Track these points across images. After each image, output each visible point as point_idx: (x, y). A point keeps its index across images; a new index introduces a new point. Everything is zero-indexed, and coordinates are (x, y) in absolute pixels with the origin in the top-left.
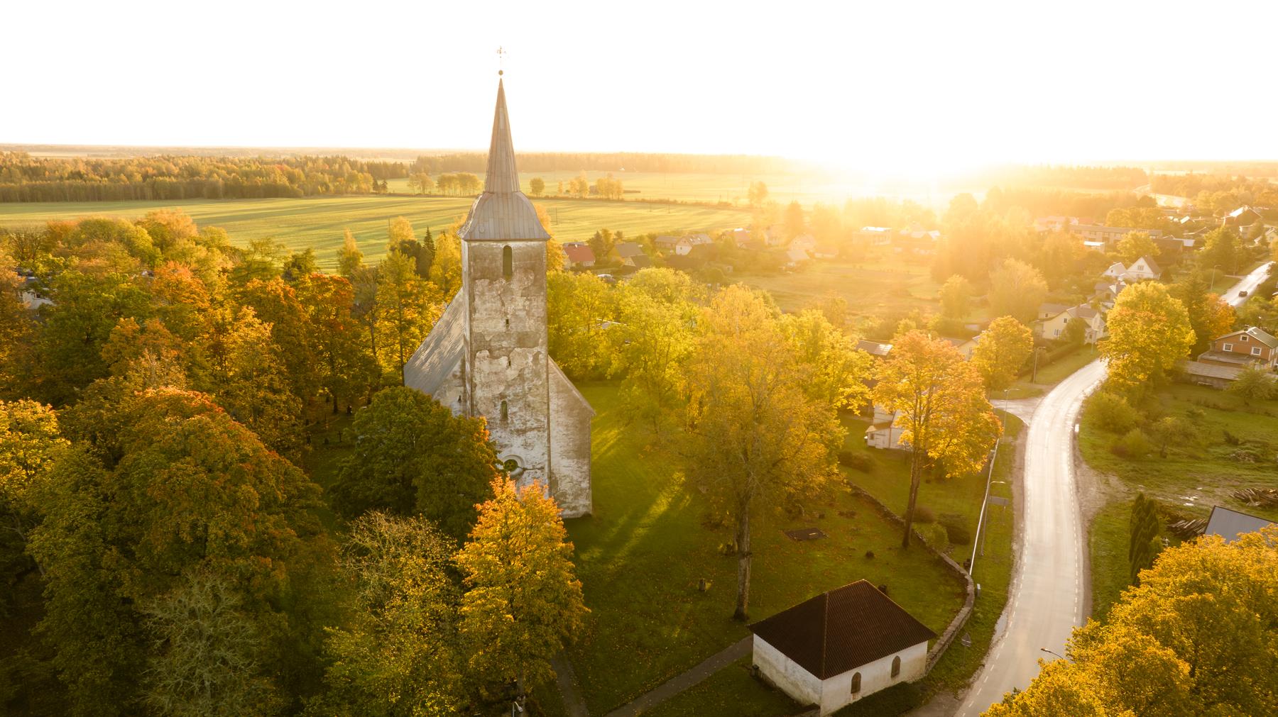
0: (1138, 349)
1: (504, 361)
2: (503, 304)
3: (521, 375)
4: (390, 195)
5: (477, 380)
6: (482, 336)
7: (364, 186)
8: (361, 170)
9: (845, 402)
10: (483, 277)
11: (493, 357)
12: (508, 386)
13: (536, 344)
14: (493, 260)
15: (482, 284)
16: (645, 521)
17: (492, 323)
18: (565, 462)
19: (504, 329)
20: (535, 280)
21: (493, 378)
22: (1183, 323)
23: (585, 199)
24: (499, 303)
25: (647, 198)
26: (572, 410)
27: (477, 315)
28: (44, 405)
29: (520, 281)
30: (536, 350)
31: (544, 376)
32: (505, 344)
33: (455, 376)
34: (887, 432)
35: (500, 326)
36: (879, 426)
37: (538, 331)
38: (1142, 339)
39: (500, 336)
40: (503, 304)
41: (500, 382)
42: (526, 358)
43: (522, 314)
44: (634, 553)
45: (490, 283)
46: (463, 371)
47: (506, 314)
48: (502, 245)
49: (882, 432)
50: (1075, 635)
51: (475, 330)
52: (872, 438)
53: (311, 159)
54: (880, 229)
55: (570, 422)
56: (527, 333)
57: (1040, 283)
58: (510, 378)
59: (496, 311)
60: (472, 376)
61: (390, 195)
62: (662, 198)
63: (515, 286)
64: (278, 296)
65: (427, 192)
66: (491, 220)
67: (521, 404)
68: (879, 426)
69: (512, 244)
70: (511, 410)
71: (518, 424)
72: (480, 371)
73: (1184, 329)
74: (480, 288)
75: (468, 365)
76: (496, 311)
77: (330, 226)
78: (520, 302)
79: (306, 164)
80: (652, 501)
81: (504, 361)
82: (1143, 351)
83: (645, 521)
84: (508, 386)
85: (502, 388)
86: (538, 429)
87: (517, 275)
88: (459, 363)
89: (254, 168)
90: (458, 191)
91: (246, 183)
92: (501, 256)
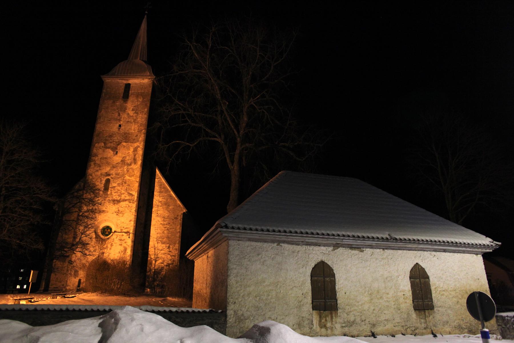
13: (134, 141)
18: (160, 246)
29: (133, 102)
30: (136, 145)
50: (114, 204)
55: (166, 214)
58: (115, 162)
67: (120, 181)
70: (113, 184)
71: (116, 197)
77: (213, 237)
86: (129, 201)
87: (131, 98)
92: (123, 87)
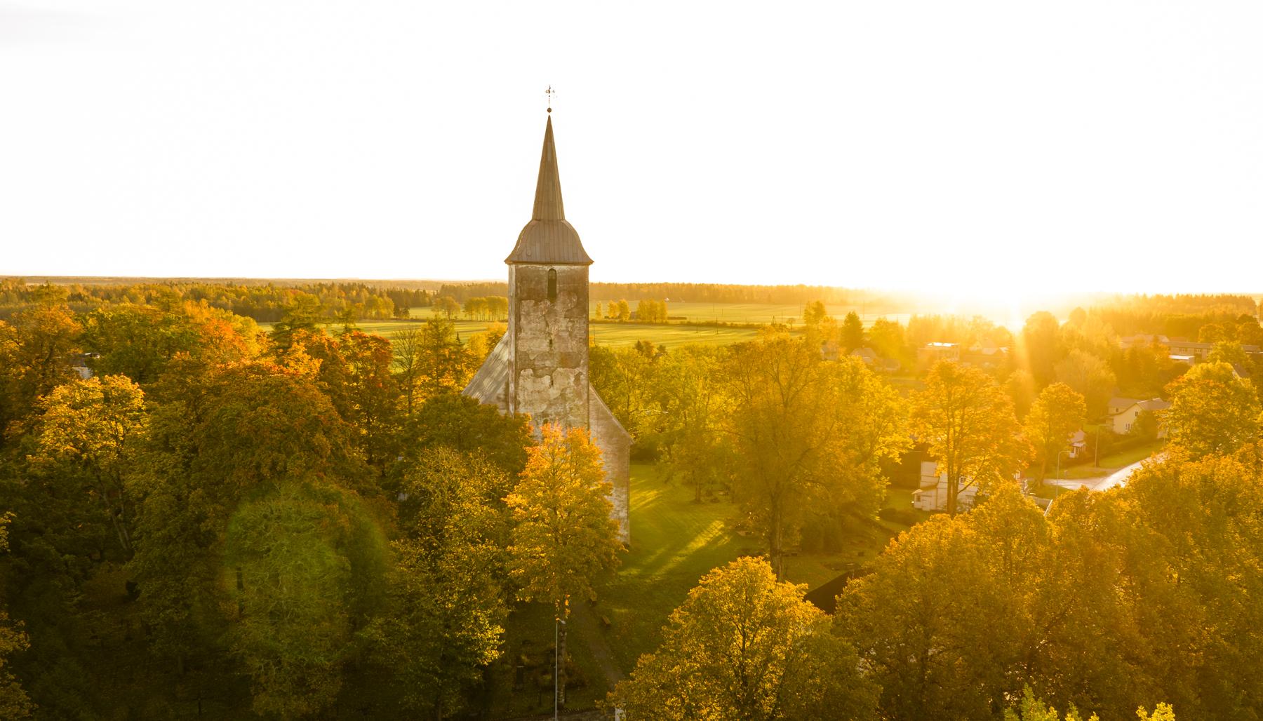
0: (1197, 417)
1: (547, 380)
2: (547, 325)
3: (563, 395)
4: (412, 320)
5: (521, 398)
6: (526, 354)
7: (384, 311)
8: (381, 295)
9: (886, 450)
10: (529, 298)
11: (537, 376)
12: (550, 405)
13: (578, 365)
14: (539, 282)
15: (527, 305)
16: (684, 552)
17: (536, 343)
19: (547, 349)
20: (578, 303)
21: (536, 396)
22: (1253, 402)
23: (626, 323)
24: (543, 324)
25: (694, 321)
26: (611, 437)
27: (522, 335)
28: (133, 383)
29: (564, 303)
30: (577, 370)
31: (585, 397)
32: (548, 363)
33: (498, 398)
34: (933, 492)
35: (545, 346)
36: (925, 489)
37: (579, 352)
38: (1199, 405)
39: (543, 356)
40: (547, 325)
41: (543, 400)
42: (568, 378)
43: (565, 335)
44: (671, 573)
45: (536, 304)
46: (507, 394)
47: (550, 334)
48: (547, 268)
49: (929, 493)
51: (520, 348)
52: (919, 500)
53: (325, 286)
54: (949, 345)
56: (569, 354)
57: (1105, 374)
58: (553, 397)
59: (540, 331)
60: (516, 394)
61: (412, 320)
62: (713, 319)
63: (559, 307)
64: (323, 345)
65: (452, 317)
66: (538, 245)
68: (925, 489)
69: (557, 268)
72: (524, 389)
73: (1254, 409)
74: (526, 308)
75: (512, 386)
76: (540, 331)
78: (564, 323)
79: (321, 290)
80: (692, 539)
81: (547, 380)
82: (1203, 419)
83: (684, 552)
84: (550, 405)
85: (544, 407)
87: (561, 298)
88: (503, 386)
89: (264, 292)
90: (486, 317)
91: (256, 307)
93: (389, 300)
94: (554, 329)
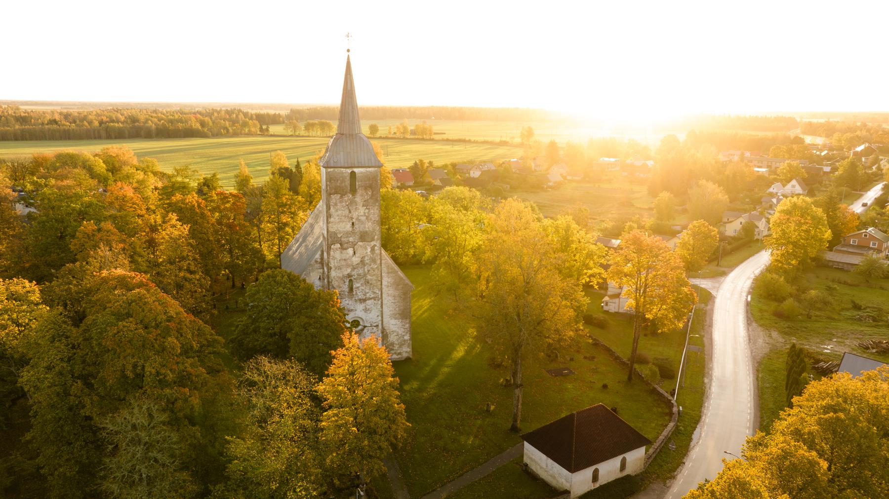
0: (792, 243)
1: (350, 251)
2: (350, 212)
3: (362, 261)
4: (271, 136)
5: (332, 265)
6: (335, 234)
7: (253, 129)
8: (251, 119)
9: (588, 280)
10: (336, 193)
11: (343, 248)
12: (354, 269)
13: (373, 240)
14: (343, 181)
15: (335, 198)
16: (449, 362)
17: (342, 225)
18: (393, 321)
19: (351, 229)
20: (372, 195)
21: (343, 263)
22: (823, 225)
23: (407, 139)
24: (347, 211)
25: (450, 138)
26: (398, 285)
27: (332, 220)
28: (30, 282)
29: (362, 195)
30: (373, 243)
31: (379, 262)
32: (351, 239)
33: (316, 262)
34: (617, 300)
35: (348, 227)
36: (612, 297)
37: (374, 230)
38: (794, 236)
39: (348, 234)
40: (350, 212)
41: (348, 266)
42: (366, 249)
43: (363, 218)
44: (441, 385)
45: (341, 197)
46: (322, 258)
47: (352, 218)
48: (349, 171)
49: (614, 301)
50: (748, 442)
51: (331, 230)
52: (607, 305)
53: (216, 111)
54: (612, 160)
55: (397, 293)
56: (366, 232)
57: (723, 197)
58: (355, 263)
59: (345, 216)
60: (329, 262)
61: (271, 136)
62: (461, 138)
63: (358, 199)
64: (194, 206)
65: (297, 134)
66: (342, 153)
67: (362, 281)
68: (612, 297)
69: (356, 170)
70: (356, 285)
71: (360, 295)
72: (334, 258)
73: (823, 229)
74: (334, 201)
75: (325, 254)
76: (345, 216)
77: (230, 157)
78: (362, 210)
79: (213, 114)
80: (454, 348)
81: (350, 251)
82: (795, 244)
83: (449, 362)
84: (354, 269)
85: (349, 270)
86: (374, 298)
87: (360, 192)
88: (319, 253)
89: (177, 117)
90: (319, 133)
91: (171, 128)
92: (348, 178)
93: (256, 122)
94: (355, 215)
